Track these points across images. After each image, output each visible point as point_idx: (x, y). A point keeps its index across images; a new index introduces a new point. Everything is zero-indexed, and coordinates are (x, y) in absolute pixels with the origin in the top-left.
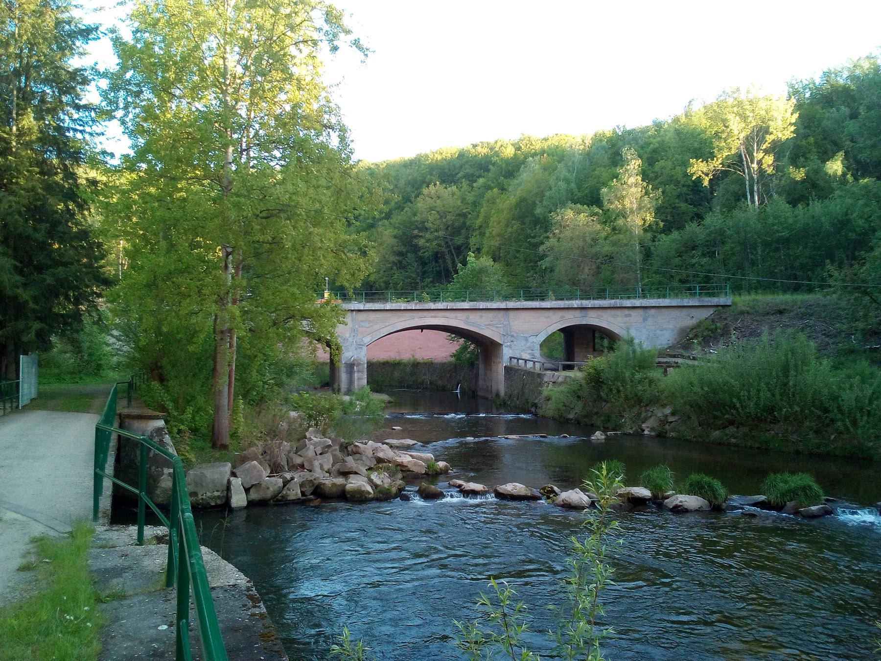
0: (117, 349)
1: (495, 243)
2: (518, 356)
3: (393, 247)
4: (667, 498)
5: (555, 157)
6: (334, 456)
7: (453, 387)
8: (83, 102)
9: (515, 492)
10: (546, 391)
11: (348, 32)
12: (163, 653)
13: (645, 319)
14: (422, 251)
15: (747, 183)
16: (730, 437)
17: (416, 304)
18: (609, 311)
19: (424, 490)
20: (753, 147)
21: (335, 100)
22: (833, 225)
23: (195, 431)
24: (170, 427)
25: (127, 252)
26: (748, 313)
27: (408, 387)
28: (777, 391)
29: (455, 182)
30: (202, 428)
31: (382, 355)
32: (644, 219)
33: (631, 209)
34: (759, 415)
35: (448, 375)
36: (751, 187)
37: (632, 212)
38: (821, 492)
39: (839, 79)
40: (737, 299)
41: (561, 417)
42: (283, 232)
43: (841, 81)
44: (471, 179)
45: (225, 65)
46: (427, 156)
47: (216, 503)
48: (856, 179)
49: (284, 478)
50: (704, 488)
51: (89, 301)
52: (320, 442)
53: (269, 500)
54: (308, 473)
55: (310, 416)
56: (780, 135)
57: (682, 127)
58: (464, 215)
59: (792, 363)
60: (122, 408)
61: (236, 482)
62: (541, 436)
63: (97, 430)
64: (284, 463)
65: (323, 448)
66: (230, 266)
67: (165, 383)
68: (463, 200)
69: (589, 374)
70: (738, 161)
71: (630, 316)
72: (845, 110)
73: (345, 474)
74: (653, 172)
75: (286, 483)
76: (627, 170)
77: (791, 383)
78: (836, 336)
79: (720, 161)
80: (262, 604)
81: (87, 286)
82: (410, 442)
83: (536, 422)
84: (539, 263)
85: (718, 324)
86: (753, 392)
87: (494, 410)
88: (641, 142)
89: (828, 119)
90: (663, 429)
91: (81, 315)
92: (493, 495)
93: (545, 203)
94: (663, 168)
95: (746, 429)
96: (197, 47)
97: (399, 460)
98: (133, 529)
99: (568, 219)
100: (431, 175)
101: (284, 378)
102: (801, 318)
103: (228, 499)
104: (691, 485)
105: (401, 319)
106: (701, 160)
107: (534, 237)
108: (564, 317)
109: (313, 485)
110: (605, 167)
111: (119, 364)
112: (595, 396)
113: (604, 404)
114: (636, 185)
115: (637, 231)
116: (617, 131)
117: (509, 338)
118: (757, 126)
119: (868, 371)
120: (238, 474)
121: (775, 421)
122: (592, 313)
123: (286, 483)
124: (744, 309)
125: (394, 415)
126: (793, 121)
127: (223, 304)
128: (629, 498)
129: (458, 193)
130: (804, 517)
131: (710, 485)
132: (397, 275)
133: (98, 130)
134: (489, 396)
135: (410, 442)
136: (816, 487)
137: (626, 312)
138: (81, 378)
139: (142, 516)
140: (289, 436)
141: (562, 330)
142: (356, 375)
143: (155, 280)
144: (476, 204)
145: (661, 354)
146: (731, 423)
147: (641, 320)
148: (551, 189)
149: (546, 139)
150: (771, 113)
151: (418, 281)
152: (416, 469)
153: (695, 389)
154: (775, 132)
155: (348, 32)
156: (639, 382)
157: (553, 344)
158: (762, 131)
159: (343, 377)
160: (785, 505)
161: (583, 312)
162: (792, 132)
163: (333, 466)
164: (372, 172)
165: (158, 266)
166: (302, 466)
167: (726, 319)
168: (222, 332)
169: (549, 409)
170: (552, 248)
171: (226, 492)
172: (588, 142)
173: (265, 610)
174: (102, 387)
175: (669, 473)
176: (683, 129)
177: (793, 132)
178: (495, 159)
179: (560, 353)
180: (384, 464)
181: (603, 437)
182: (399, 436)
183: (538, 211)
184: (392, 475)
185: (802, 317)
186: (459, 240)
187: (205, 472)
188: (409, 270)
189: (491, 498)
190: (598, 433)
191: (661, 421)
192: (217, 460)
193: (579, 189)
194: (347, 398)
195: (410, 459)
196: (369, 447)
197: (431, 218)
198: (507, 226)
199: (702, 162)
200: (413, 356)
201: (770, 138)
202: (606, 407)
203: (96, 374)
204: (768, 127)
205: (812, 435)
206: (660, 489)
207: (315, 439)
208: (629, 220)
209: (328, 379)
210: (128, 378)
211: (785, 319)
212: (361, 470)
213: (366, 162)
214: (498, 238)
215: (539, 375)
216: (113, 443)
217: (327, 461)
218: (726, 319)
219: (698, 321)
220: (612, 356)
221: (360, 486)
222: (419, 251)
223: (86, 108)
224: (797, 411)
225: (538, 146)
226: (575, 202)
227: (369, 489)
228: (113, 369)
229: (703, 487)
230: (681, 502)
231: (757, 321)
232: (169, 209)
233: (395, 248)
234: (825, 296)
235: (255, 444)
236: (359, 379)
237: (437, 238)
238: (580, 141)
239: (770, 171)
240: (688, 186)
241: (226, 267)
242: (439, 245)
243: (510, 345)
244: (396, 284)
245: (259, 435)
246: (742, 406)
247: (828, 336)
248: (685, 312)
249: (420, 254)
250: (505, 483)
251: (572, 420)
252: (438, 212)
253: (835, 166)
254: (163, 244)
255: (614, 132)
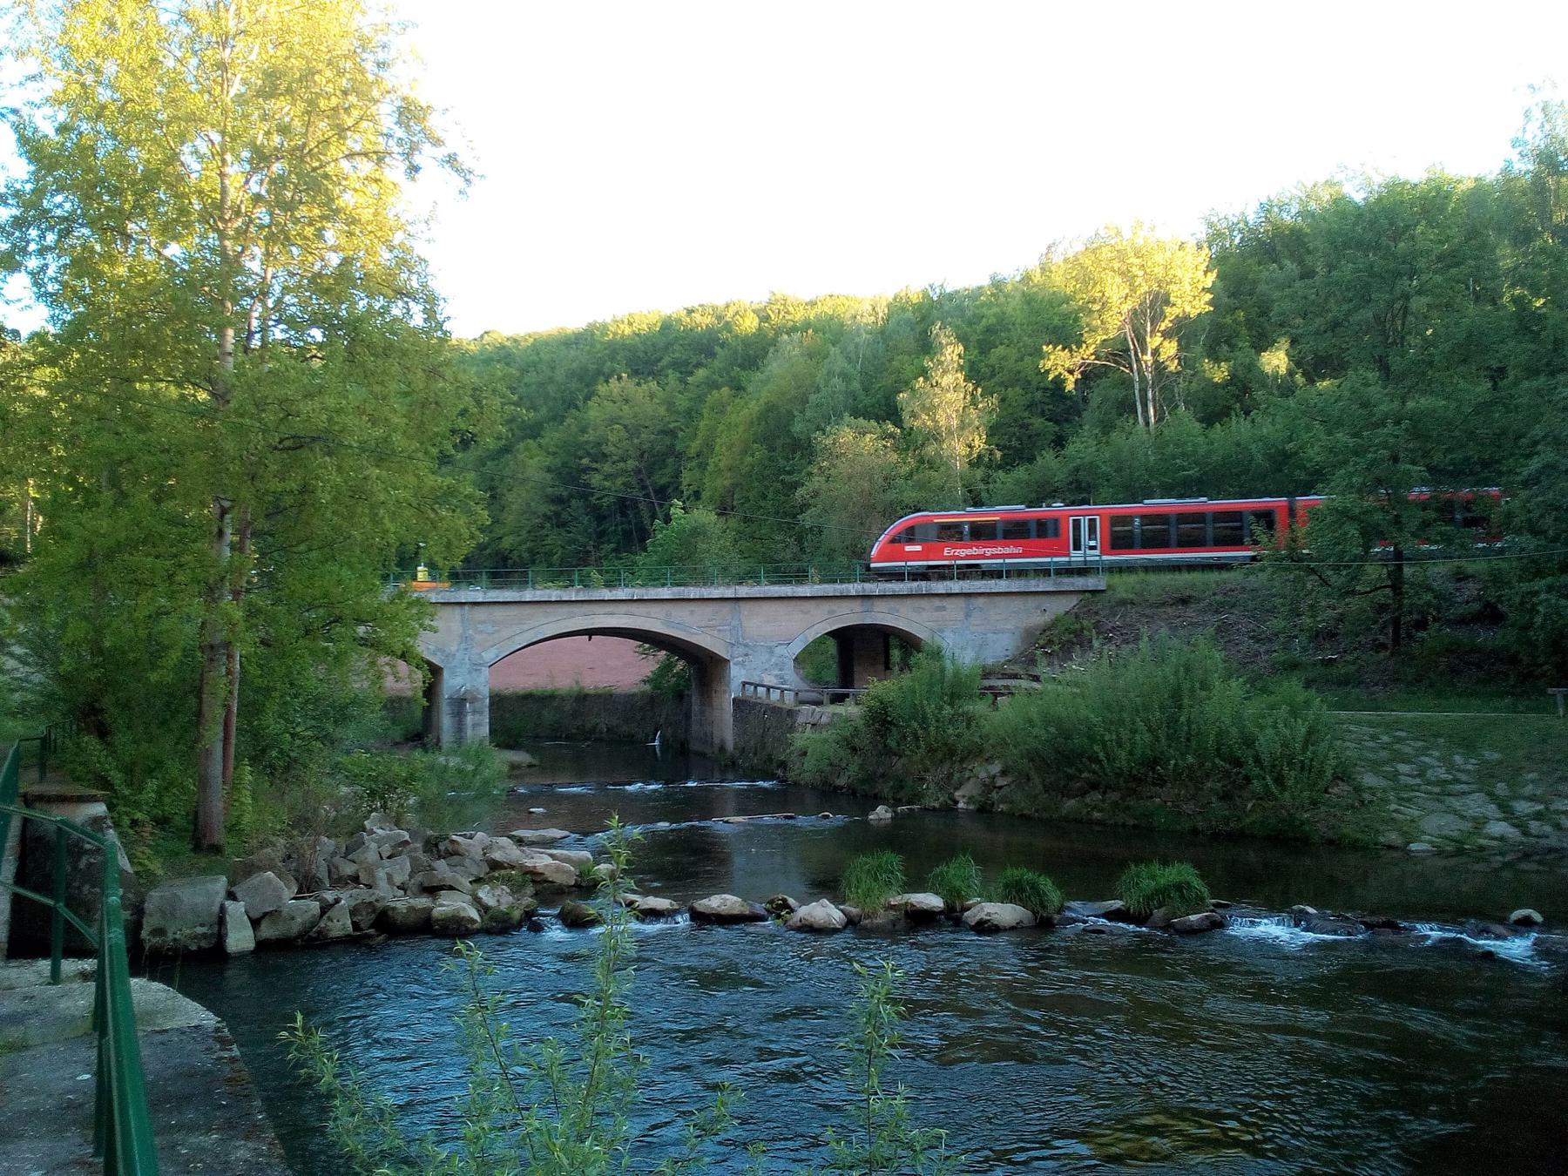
1: (724, 482)
2: (756, 680)
6: (414, 860)
7: (647, 735)
9: (724, 910)
10: (802, 738)
11: (437, 142)
12: (81, 1105)
13: (968, 616)
15: (1137, 386)
16: (1093, 809)
17: (578, 591)
18: (908, 602)
19: (570, 912)
21: (420, 249)
23: (162, 822)
24: (116, 816)
25: (40, 507)
26: (1132, 603)
27: (567, 738)
28: (1162, 734)
29: (655, 374)
31: (520, 681)
32: (970, 446)
34: (1135, 772)
36: (1143, 391)
37: (950, 433)
38: (1205, 891)
39: (1284, 215)
41: (825, 783)
42: (317, 478)
43: (1287, 219)
45: (222, 183)
47: (199, 947)
48: (1311, 381)
49: (322, 900)
50: (1025, 891)
55: (373, 794)
56: (1188, 309)
57: (1035, 290)
58: (672, 433)
59: (1186, 685)
61: (236, 910)
62: (786, 817)
64: (322, 873)
65: (394, 847)
66: (228, 531)
68: (670, 405)
69: (870, 709)
70: (1119, 352)
71: (944, 608)
73: (432, 890)
74: (986, 366)
75: (326, 908)
76: (941, 363)
77: (1183, 719)
79: (1091, 350)
82: (556, 833)
83: (784, 792)
84: (800, 517)
85: (1085, 623)
86: (1125, 734)
87: (717, 775)
88: (969, 314)
93: (808, 414)
94: (1004, 358)
95: (1114, 796)
97: (529, 863)
98: (44, 965)
100: (613, 359)
102: (1217, 612)
103: (221, 938)
104: (1006, 886)
105: (550, 619)
106: (1060, 347)
107: (790, 473)
108: (833, 612)
109: (374, 911)
112: (880, 747)
113: (895, 759)
116: (931, 294)
117: (741, 650)
119: (1300, 698)
120: (239, 895)
121: (1161, 781)
122: (881, 606)
123: (326, 908)
124: (1125, 595)
127: (214, 600)
130: (1178, 932)
131: (1034, 886)
132: (554, 538)
134: (709, 751)
135: (556, 833)
136: (1197, 883)
137: (937, 602)
139: (58, 942)
140: (333, 829)
141: (833, 634)
142: (469, 719)
144: (691, 414)
145: (987, 674)
146: (1094, 786)
147: (961, 616)
148: (818, 390)
149: (813, 304)
151: (590, 548)
152: (560, 879)
153: (1035, 731)
154: (1179, 302)
155: (437, 142)
156: (951, 721)
158: (1159, 301)
159: (446, 722)
160: (1151, 914)
161: (868, 603)
162: (1206, 303)
163: (411, 876)
164: (501, 356)
166: (355, 879)
169: (806, 771)
170: (816, 494)
172: (882, 312)
175: (974, 869)
177: (1210, 303)
178: (725, 335)
179: (832, 674)
180: (503, 872)
181: (889, 815)
182: (537, 823)
183: (798, 427)
184: (516, 889)
186: (662, 478)
187: (179, 893)
188: (574, 530)
189: (683, 921)
190: (881, 809)
191: (985, 785)
192: (204, 871)
193: (866, 390)
194: (454, 762)
195: (550, 861)
196: (476, 842)
197: (612, 438)
198: (745, 452)
199: (1064, 349)
200: (577, 683)
201: (1171, 313)
202: (899, 764)
204: (1167, 295)
208: (945, 446)
211: (1190, 612)
213: (495, 336)
215: (791, 713)
217: (401, 870)
220: (906, 679)
221: (458, 910)
222: (592, 494)
225: (799, 316)
226: (856, 413)
227: (474, 914)
228: (14, 715)
229: (1023, 890)
230: (989, 914)
231: (1147, 616)
232: (117, 434)
234: (1247, 575)
235: (271, 842)
236: (475, 726)
237: (624, 472)
238: (870, 308)
239: (1173, 366)
240: (1046, 389)
241: (221, 533)
244: (550, 554)
245: (278, 827)
248: (1032, 602)
249: (593, 499)
251: (843, 787)
252: (625, 427)
253: (1276, 360)
254: (108, 495)
255: (925, 294)
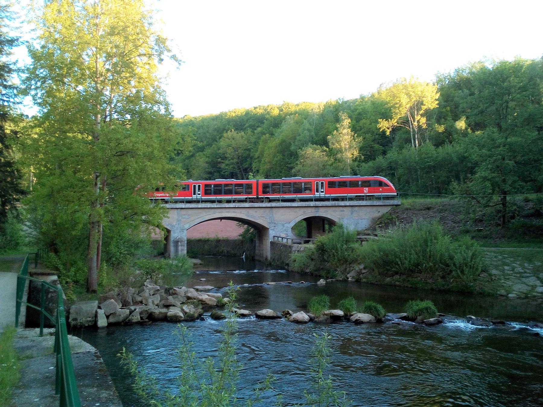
0: (28, 233)
1: (268, 166)
2: (278, 235)
3: (205, 169)
4: (352, 315)
5: (303, 116)
6: (161, 296)
8: (9, 83)
11: (169, 51)
13: (352, 213)
14: (223, 172)
15: (412, 133)
18: (331, 208)
20: (414, 112)
21: (163, 87)
22: (459, 159)
23: (76, 282)
27: (213, 255)
30: (81, 281)
31: (197, 235)
33: (345, 148)
34: (411, 268)
35: (238, 247)
36: (414, 135)
37: (346, 150)
38: (436, 310)
39: (464, 73)
40: (405, 201)
41: (302, 271)
42: (129, 165)
43: (465, 75)
44: (253, 128)
46: (226, 113)
49: (130, 309)
51: (11, 204)
52: (153, 288)
53: (121, 322)
54: (145, 306)
56: (430, 106)
57: (376, 100)
58: (249, 150)
60: (32, 269)
61: (101, 312)
63: (18, 278)
64: (130, 300)
67: (58, 254)
69: (318, 246)
70: (406, 121)
71: (343, 211)
72: (466, 91)
73: (167, 306)
74: (359, 126)
75: (131, 312)
76: (342, 125)
77: (428, 250)
78: (459, 222)
79: (396, 121)
80: (101, 359)
81: (10, 195)
89: (458, 97)
90: (359, 277)
91: (6, 213)
92: (255, 316)
93: (296, 143)
94: (365, 124)
96: (80, 56)
97: (200, 297)
98: (38, 330)
99: (309, 153)
100: (229, 125)
101: (133, 250)
102: (440, 212)
103: (96, 322)
104: (365, 308)
107: (290, 164)
109: (148, 313)
110: (332, 122)
111: (30, 242)
112: (321, 259)
114: (348, 134)
115: (349, 161)
116: (339, 101)
117: (273, 225)
118: (416, 101)
119: (470, 243)
120: (102, 307)
121: (420, 272)
123: (131, 312)
125: (202, 272)
126: (437, 98)
128: (331, 316)
129: (245, 136)
130: (426, 325)
131: (375, 308)
133: (18, 101)
134: (261, 259)
137: (341, 209)
138: (5, 251)
140: (134, 285)
142: (180, 248)
143: (52, 192)
144: (256, 143)
145: (359, 234)
146: (397, 273)
149: (298, 105)
150: (424, 93)
152: (210, 303)
153: (376, 254)
155: (169, 51)
157: (301, 228)
158: (419, 104)
159: (172, 249)
160: (417, 318)
163: (160, 301)
164: (190, 123)
165: (54, 184)
166: (141, 302)
167: (397, 213)
168: (93, 223)
169: (295, 267)
171: (94, 318)
172: (322, 108)
173: (103, 361)
174: (19, 256)
175: (354, 302)
176: (376, 101)
177: (437, 104)
178: (267, 116)
179: (304, 233)
181: (324, 283)
183: (293, 148)
184: (196, 306)
185: (440, 211)
186: (246, 165)
189: (253, 318)
190: (322, 280)
192: (90, 299)
194: (175, 262)
195: (207, 297)
196: (182, 290)
197: (229, 151)
198: (274, 157)
201: (424, 108)
202: (328, 265)
203: (15, 249)
204: (422, 101)
205: (440, 280)
206: (349, 311)
207: (149, 286)
208: (344, 154)
209: (163, 251)
210: (35, 251)
211: (431, 213)
212: (177, 304)
214: (269, 164)
216: (26, 289)
217: (157, 299)
218: (397, 213)
219: (382, 214)
220: (330, 235)
222: (222, 171)
223: (10, 87)
224: (431, 266)
225: (293, 109)
226: (313, 143)
230: (359, 317)
231: (416, 214)
233: (207, 170)
236: (182, 250)
237: (232, 163)
239: (424, 126)
240: (379, 134)
241: (96, 184)
242: (234, 168)
243: (274, 229)
245: (115, 284)
246: (401, 263)
247: (455, 223)
248: (375, 208)
249: (222, 173)
250: (261, 309)
252: (233, 148)
253: (461, 124)
254: (58, 171)
255: (337, 102)
